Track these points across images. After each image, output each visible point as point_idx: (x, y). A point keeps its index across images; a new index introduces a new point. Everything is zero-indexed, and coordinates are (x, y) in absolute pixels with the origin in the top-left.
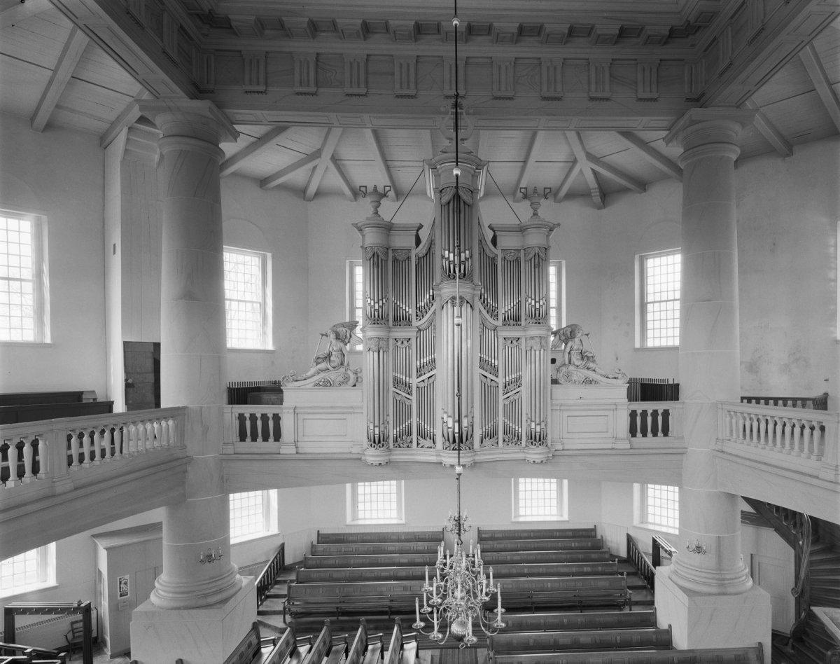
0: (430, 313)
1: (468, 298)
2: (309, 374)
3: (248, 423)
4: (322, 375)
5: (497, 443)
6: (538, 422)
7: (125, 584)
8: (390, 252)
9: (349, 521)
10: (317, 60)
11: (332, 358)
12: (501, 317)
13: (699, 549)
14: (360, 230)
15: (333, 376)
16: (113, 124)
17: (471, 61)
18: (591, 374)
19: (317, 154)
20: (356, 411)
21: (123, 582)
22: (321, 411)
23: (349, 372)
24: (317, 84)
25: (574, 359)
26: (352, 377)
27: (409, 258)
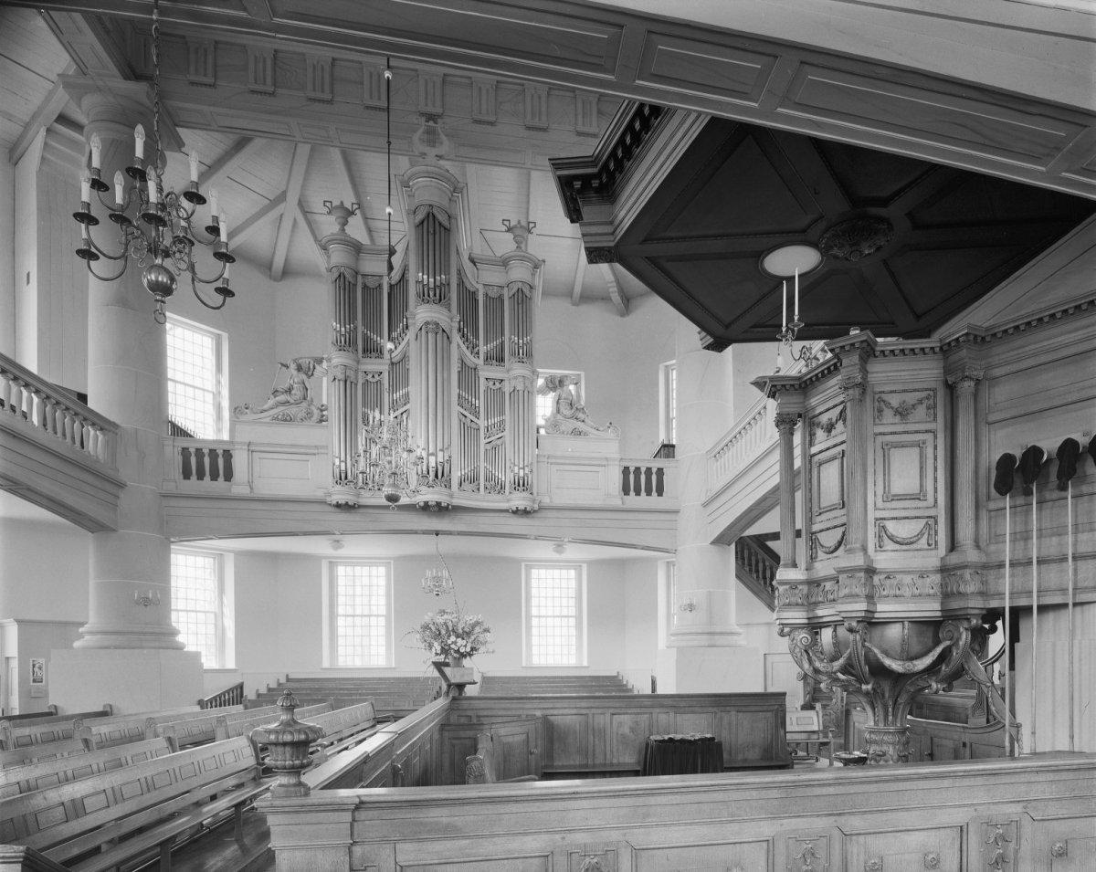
0: (403, 344)
1: (444, 325)
2: (266, 407)
3: (193, 460)
4: (282, 408)
5: (479, 489)
6: (521, 466)
7: (40, 668)
8: (359, 277)
9: (326, 664)
10: (275, 58)
11: (293, 392)
12: (482, 355)
13: (691, 607)
14: (325, 248)
15: (293, 410)
16: (27, 126)
17: (449, 79)
18: (580, 425)
19: (282, 198)
20: (320, 451)
21: (37, 665)
22: (279, 449)
23: (313, 408)
24: (275, 84)
25: (562, 409)
26: (316, 412)
27: (380, 286)
